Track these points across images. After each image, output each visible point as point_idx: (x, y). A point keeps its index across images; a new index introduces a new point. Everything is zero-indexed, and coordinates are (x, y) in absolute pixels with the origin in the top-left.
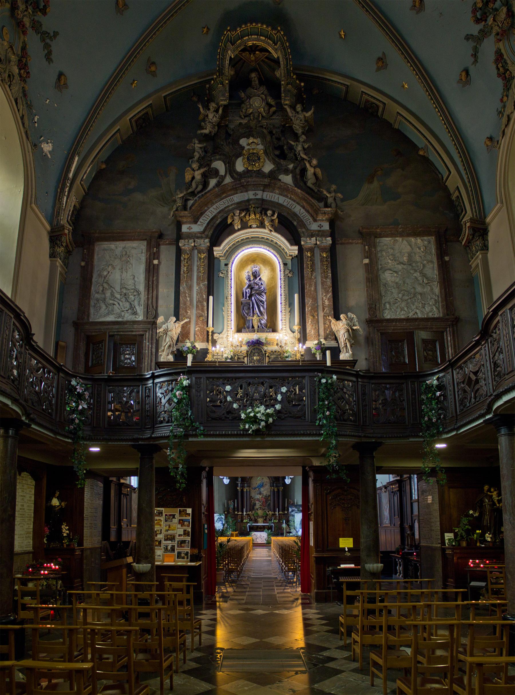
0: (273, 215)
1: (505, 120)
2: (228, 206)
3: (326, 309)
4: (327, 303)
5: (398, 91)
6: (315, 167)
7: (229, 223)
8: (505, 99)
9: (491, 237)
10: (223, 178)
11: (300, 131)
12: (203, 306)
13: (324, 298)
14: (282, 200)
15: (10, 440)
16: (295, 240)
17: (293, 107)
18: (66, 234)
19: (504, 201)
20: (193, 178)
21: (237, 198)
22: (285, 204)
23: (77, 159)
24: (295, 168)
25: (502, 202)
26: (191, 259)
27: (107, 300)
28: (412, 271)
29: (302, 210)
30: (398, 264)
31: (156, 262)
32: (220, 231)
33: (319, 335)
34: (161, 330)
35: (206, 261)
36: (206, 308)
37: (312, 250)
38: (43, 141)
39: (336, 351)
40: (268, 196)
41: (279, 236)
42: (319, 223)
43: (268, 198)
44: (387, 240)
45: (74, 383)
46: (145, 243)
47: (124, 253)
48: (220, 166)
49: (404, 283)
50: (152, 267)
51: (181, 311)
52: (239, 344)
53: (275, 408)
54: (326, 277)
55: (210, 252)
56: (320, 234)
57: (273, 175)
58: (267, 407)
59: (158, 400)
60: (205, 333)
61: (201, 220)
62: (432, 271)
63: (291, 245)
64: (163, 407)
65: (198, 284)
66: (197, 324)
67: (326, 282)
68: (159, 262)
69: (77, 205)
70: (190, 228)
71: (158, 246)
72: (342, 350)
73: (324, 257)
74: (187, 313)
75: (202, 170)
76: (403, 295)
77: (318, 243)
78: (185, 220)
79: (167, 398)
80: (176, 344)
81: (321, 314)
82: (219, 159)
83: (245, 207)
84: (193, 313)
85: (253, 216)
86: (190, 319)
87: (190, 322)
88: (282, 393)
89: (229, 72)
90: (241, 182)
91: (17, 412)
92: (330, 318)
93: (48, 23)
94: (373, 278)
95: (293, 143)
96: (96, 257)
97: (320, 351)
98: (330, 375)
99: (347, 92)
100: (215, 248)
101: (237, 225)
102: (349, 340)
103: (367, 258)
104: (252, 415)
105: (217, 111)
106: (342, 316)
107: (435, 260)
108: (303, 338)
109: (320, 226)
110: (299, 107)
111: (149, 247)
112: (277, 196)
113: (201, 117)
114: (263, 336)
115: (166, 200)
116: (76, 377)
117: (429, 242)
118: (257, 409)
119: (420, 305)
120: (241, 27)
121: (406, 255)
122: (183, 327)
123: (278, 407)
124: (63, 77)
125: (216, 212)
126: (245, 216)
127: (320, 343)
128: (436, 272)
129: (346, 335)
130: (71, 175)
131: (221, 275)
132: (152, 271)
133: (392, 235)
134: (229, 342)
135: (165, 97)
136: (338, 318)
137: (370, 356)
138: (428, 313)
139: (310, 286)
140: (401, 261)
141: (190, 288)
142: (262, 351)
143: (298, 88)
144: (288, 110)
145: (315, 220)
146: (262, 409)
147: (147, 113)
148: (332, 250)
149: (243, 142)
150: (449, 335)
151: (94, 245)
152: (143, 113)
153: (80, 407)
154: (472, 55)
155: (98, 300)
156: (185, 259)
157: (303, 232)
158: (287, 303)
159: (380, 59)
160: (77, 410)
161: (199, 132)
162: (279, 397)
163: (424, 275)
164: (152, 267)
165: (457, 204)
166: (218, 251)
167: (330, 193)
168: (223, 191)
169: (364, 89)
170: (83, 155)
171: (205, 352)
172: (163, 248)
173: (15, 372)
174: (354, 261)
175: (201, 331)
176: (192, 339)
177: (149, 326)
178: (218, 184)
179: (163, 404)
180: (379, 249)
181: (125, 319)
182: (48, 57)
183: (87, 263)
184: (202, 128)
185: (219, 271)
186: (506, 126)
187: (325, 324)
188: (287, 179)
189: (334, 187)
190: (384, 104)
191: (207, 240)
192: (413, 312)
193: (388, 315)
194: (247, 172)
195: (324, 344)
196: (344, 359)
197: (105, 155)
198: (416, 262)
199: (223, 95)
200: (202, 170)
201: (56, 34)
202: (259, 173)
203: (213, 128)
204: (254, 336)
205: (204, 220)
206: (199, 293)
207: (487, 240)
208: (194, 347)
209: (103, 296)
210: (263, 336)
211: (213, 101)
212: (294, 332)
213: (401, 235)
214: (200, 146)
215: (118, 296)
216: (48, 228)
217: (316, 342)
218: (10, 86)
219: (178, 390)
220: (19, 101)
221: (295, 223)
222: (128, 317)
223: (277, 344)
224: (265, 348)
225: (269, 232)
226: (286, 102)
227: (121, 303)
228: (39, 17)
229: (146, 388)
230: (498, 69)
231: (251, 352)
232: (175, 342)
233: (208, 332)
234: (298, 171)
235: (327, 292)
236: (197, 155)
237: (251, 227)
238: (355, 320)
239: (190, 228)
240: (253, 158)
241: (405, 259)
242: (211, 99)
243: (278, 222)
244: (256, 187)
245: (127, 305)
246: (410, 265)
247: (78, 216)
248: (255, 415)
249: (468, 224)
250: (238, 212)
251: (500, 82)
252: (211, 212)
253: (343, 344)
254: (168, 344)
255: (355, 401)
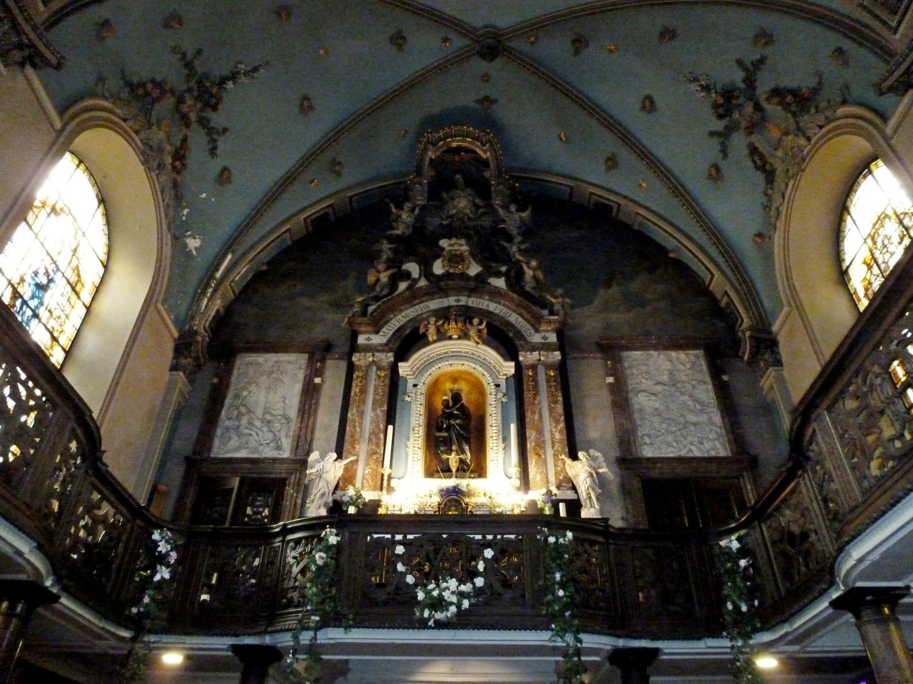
0: (480, 324)
1: (773, 213)
2: (422, 314)
3: (557, 445)
4: (558, 436)
5: (634, 192)
6: (534, 269)
7: (421, 332)
8: (770, 192)
9: (783, 350)
10: (416, 281)
11: (515, 232)
12: (379, 439)
13: (554, 430)
14: (493, 307)
15: (14, 621)
16: (511, 353)
17: (506, 207)
18: (198, 342)
19: (792, 302)
20: (378, 280)
21: (435, 304)
22: (497, 311)
23: (229, 257)
24: (508, 271)
25: (790, 305)
26: (365, 377)
27: (242, 428)
28: (677, 394)
29: (520, 319)
30: (656, 384)
31: (317, 380)
32: (408, 342)
33: (548, 482)
34: (314, 470)
35: (387, 381)
36: (382, 442)
37: (534, 367)
38: (189, 236)
39: (574, 506)
40: (473, 302)
41: (489, 350)
42: (543, 334)
43: (474, 305)
44: (636, 354)
45: (156, 536)
46: (306, 356)
47: (275, 369)
48: (413, 268)
49: (667, 407)
50: (311, 388)
51: (347, 446)
52: (428, 494)
53: (474, 584)
54: (556, 402)
55: (394, 369)
56: (546, 347)
57: (480, 279)
58: (461, 581)
59: (287, 568)
60: (379, 477)
61: (384, 330)
62: (706, 393)
63: (506, 360)
64: (293, 580)
65: (374, 410)
66: (367, 465)
67: (555, 408)
68: (322, 381)
69: (222, 311)
70: (368, 339)
71: (323, 360)
72: (583, 504)
73: (551, 376)
74: (354, 448)
75: (390, 272)
76: (669, 425)
77: (542, 358)
78: (363, 329)
79: (301, 565)
80: (334, 493)
81: (550, 452)
82: (413, 261)
83: (444, 314)
84: (362, 449)
85: (453, 324)
86: (358, 456)
87: (357, 461)
88: (485, 560)
89: (428, 172)
90: (438, 286)
91: (36, 569)
92: (563, 457)
93: (217, 119)
94: (621, 401)
95: (505, 244)
96: (235, 372)
97: (550, 505)
98: (562, 532)
99: (571, 194)
100: (400, 364)
101: (432, 335)
102: (593, 489)
103: (611, 375)
104: (435, 593)
105: (412, 211)
106: (581, 454)
107: (708, 379)
108: (525, 482)
109: (545, 338)
110: (513, 208)
111: (311, 361)
112: (486, 303)
113: (393, 217)
114: (464, 483)
115: (339, 306)
116: (161, 527)
117: (697, 357)
118: (444, 585)
119: (696, 439)
120: (443, 129)
121: (666, 372)
122: (347, 468)
123: (479, 582)
124: (226, 173)
125: (405, 320)
126: (443, 325)
127: (549, 493)
128: (712, 394)
129: (589, 481)
130: (218, 275)
131: (407, 399)
132: (310, 392)
133: (643, 348)
134: (410, 487)
135: (350, 198)
136: (574, 457)
137: (628, 513)
138: (708, 451)
139: (533, 413)
140: (660, 379)
141: (361, 414)
142: (461, 504)
143: (512, 189)
144: (500, 210)
145: (537, 331)
146: (453, 583)
147: (326, 214)
148: (562, 369)
149: (444, 243)
150: (747, 482)
151: (235, 358)
152: (322, 212)
153: (157, 578)
154: (720, 151)
155: (227, 429)
156: (358, 377)
157: (522, 346)
158: (501, 437)
159: (608, 159)
160: (152, 582)
161: (390, 232)
162: (481, 566)
163: (696, 400)
164: (311, 388)
165: (729, 311)
166: (404, 369)
167: (556, 297)
168: (414, 296)
169: (592, 190)
170: (239, 253)
171: (377, 504)
172: (329, 363)
173: (56, 505)
174: (593, 381)
175: (374, 473)
176: (358, 484)
177: (298, 466)
178: (409, 288)
179: (293, 575)
180: (626, 365)
181: (263, 456)
182: (213, 152)
183: (221, 382)
184: (393, 229)
185: (405, 393)
186: (777, 219)
187: (556, 466)
188: (500, 283)
189: (560, 291)
190: (619, 205)
191: (391, 354)
192: (686, 449)
193: (648, 452)
194: (447, 276)
195: (556, 495)
196: (588, 517)
197: (266, 256)
198: (682, 382)
199: (421, 195)
200: (390, 272)
201: (225, 130)
202: (464, 276)
203: (408, 227)
204: (450, 483)
205: (388, 331)
206: (375, 421)
207: (779, 353)
208: (360, 496)
209: (237, 423)
210: (464, 483)
211: (408, 201)
212: (510, 478)
213: (656, 348)
214: (389, 246)
215: (258, 424)
216: (176, 335)
217: (544, 491)
218: (157, 176)
219: (320, 551)
220: (167, 190)
221: (511, 335)
222: (269, 453)
223: (485, 494)
224: (467, 500)
225: (474, 345)
226: (497, 202)
227: (260, 433)
228: (209, 114)
229: (271, 549)
230: (754, 162)
231: (445, 505)
232: (332, 488)
233: (383, 475)
234: (512, 274)
235: (557, 422)
236: (385, 257)
237: (450, 338)
238: (601, 459)
239: (368, 339)
240: (455, 259)
241: (665, 378)
242: (407, 199)
243: (488, 333)
244: (459, 291)
245: (270, 436)
246: (674, 385)
247: (221, 322)
248: (440, 595)
249: (748, 333)
250: (434, 319)
251: (760, 177)
252: (398, 321)
253: (584, 494)
254: (322, 491)
255: (605, 576)
